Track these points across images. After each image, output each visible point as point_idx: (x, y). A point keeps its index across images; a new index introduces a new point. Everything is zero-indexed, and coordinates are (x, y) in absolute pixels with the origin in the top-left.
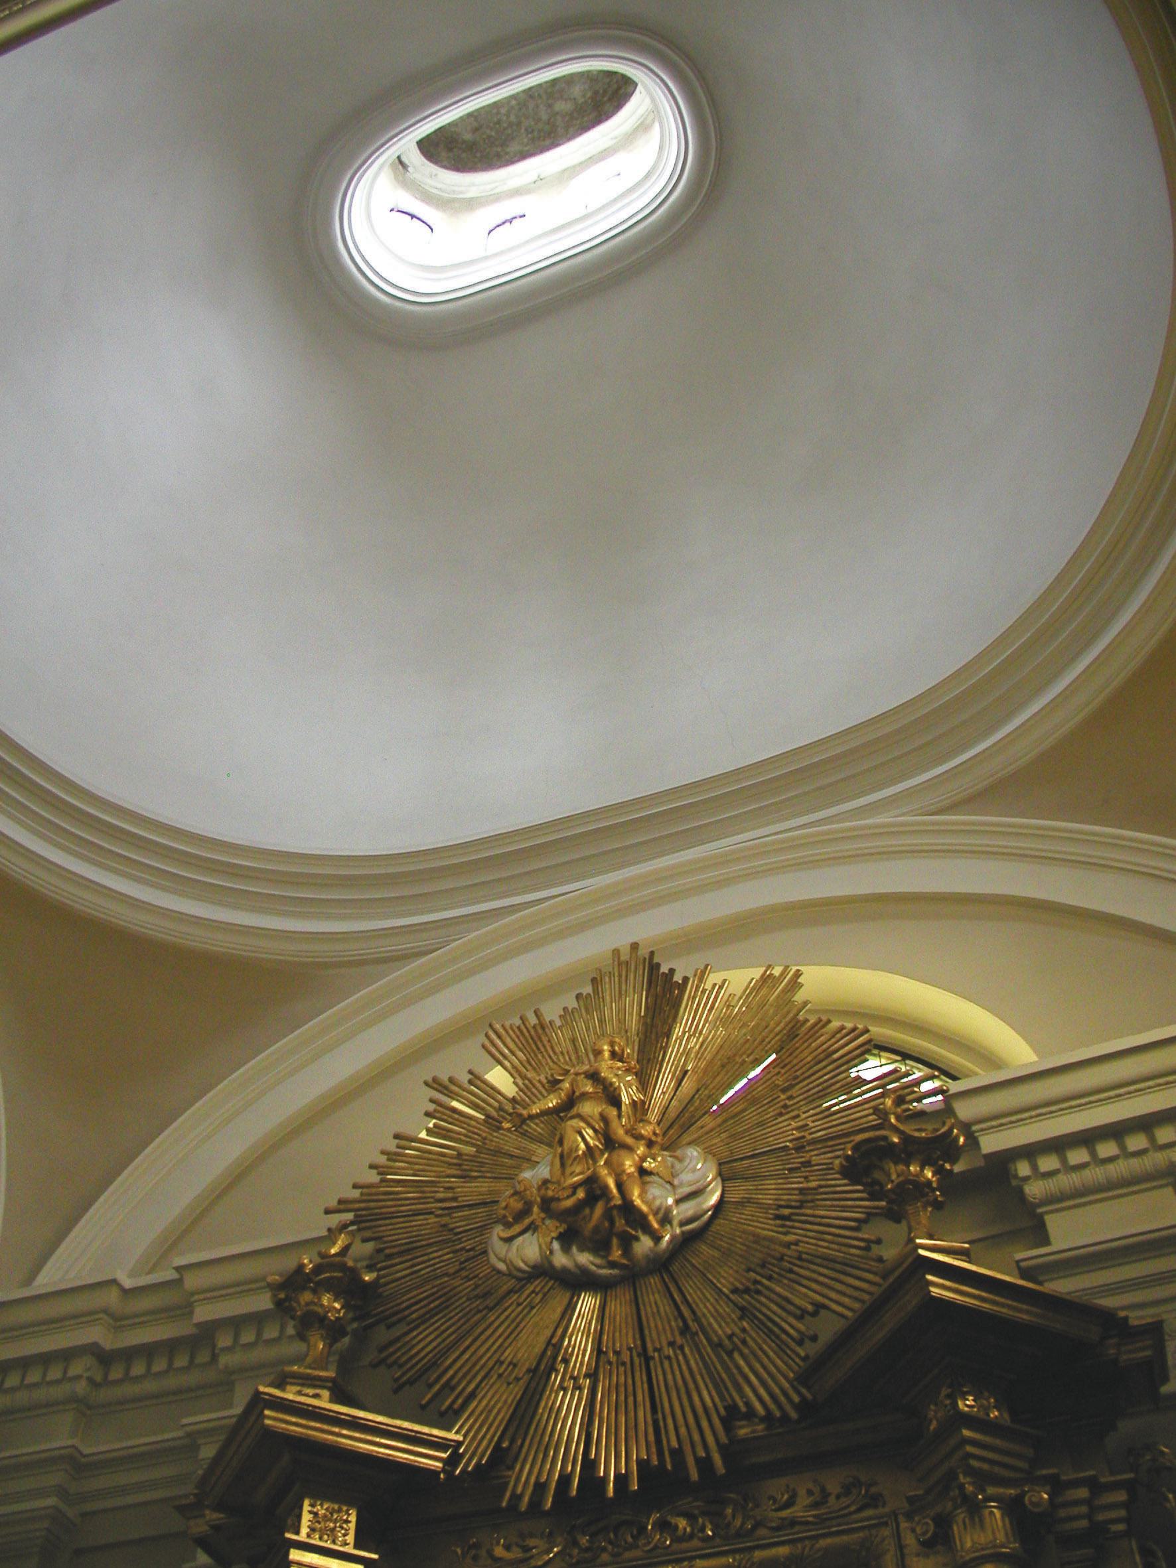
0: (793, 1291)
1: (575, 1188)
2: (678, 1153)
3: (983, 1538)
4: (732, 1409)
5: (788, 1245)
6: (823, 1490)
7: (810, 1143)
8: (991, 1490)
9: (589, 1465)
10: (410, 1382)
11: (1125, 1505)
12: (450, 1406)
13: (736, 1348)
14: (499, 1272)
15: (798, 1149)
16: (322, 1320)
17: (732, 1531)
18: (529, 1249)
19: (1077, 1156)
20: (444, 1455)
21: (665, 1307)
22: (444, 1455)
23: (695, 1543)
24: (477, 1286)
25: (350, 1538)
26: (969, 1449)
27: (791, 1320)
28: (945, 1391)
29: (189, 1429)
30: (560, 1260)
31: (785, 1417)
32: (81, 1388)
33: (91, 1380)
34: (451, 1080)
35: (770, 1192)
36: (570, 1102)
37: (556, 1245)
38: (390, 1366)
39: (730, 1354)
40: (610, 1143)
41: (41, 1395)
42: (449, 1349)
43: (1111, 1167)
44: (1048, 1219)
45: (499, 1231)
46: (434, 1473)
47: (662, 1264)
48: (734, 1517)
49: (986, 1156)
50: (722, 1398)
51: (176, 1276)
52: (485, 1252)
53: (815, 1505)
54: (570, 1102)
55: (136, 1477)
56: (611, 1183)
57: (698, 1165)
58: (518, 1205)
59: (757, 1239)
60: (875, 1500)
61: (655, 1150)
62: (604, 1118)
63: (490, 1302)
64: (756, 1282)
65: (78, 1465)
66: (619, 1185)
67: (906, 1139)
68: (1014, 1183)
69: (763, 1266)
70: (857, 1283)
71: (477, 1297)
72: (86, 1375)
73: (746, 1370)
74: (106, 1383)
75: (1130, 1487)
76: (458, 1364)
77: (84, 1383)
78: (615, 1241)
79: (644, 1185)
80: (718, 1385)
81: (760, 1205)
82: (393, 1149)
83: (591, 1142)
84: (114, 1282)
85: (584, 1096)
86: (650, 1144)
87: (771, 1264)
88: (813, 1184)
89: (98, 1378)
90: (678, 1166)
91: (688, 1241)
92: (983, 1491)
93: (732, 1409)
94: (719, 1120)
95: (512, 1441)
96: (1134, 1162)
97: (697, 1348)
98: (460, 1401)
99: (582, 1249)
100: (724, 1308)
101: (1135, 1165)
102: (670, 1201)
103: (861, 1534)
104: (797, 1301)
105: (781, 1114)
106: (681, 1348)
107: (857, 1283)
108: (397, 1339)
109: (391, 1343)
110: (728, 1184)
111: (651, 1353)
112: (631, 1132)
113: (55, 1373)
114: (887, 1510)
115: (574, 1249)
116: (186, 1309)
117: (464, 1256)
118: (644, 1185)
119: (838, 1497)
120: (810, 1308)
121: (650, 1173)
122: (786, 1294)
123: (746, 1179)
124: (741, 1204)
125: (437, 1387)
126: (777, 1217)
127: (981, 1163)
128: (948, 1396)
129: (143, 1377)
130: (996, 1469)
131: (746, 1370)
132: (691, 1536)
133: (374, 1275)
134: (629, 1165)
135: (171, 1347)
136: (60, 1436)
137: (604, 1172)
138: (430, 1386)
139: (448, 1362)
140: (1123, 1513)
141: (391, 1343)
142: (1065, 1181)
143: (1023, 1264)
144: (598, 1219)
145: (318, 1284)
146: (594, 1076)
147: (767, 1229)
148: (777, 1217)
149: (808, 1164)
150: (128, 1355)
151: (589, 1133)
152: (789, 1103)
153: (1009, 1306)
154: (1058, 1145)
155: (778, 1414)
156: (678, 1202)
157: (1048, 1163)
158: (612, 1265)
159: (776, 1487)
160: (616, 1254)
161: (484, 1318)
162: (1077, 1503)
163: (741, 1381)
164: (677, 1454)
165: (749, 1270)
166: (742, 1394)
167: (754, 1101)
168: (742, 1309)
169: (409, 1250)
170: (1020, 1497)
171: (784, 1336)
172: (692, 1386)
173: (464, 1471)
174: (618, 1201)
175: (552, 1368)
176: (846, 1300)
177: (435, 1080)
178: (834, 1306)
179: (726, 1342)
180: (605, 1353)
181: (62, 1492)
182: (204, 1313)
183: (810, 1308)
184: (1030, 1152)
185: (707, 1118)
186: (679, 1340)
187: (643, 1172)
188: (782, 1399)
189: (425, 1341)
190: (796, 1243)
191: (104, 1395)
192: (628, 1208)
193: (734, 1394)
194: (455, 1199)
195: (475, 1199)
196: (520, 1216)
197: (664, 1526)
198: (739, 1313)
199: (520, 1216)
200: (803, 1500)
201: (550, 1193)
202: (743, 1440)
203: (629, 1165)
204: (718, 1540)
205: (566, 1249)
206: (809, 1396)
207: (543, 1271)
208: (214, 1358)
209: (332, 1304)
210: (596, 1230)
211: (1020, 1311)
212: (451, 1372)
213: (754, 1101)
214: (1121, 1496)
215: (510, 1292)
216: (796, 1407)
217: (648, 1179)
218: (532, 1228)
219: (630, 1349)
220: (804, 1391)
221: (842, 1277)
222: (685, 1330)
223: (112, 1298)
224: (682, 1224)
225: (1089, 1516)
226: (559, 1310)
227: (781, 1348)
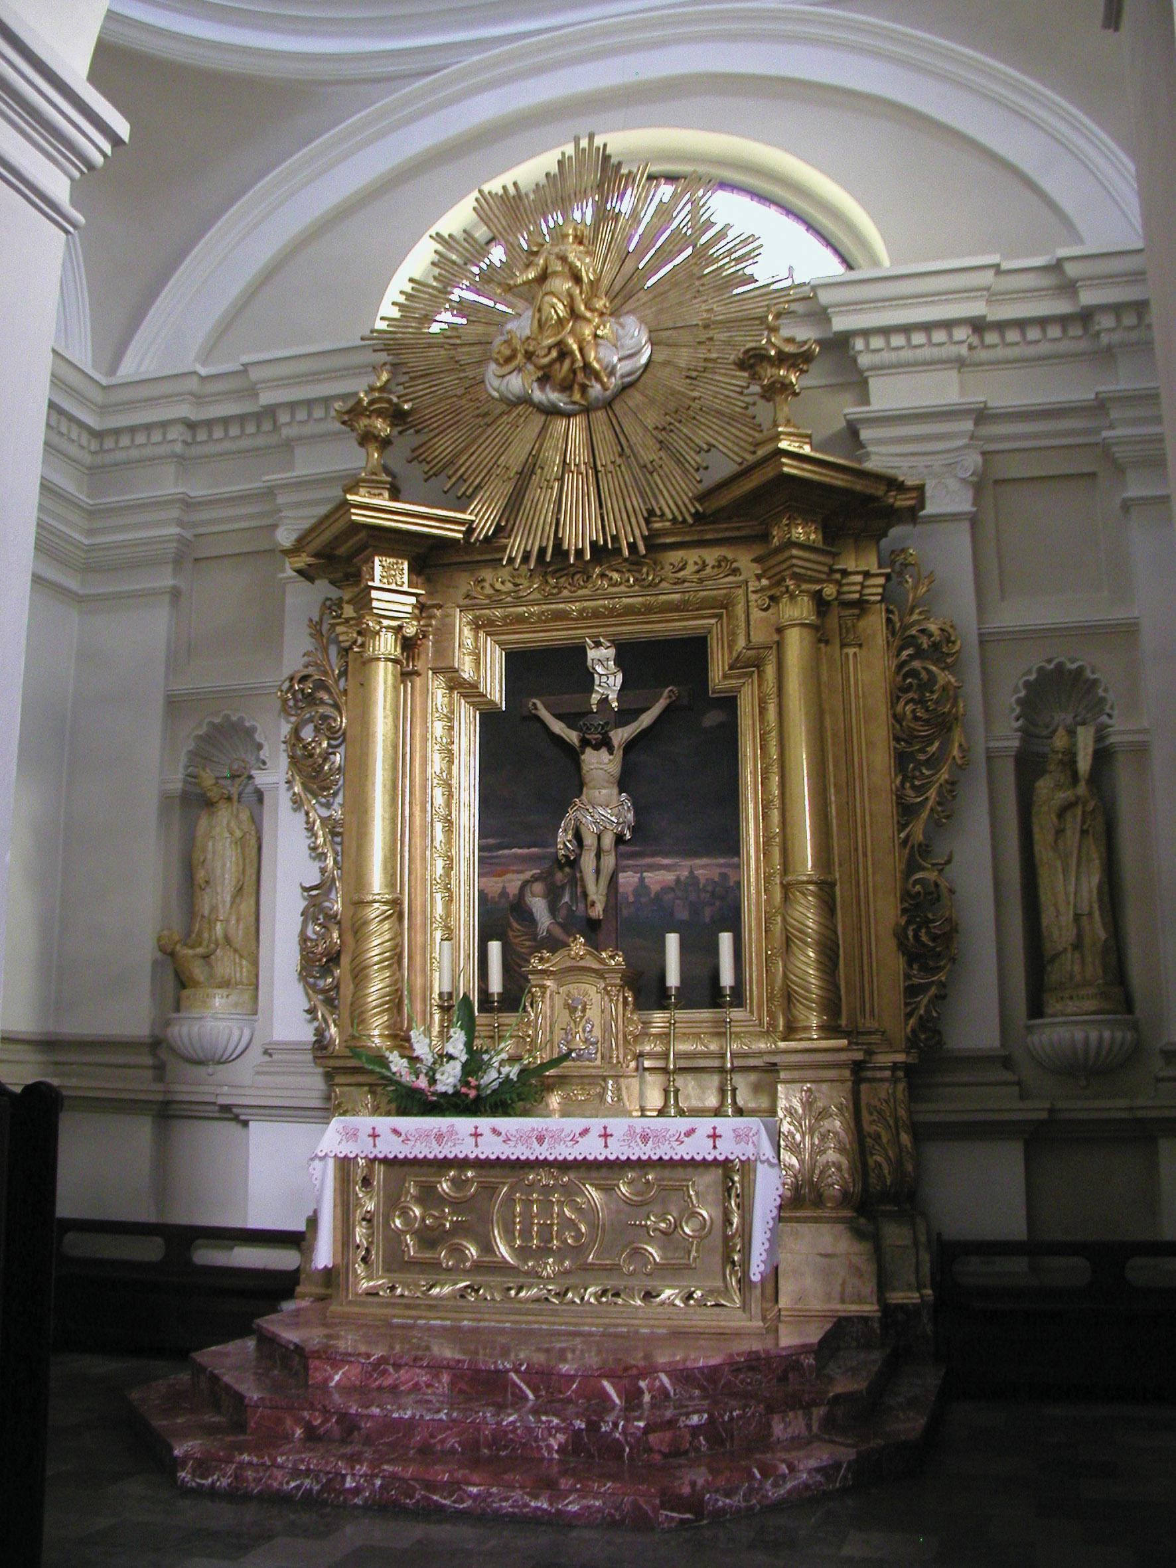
0: (695, 433)
1: (550, 349)
2: (622, 320)
3: (797, 613)
4: (651, 512)
5: (694, 399)
6: (704, 562)
7: (714, 322)
8: (804, 587)
9: (558, 542)
10: (435, 475)
11: (884, 586)
12: (464, 493)
13: (655, 470)
14: (493, 398)
15: (706, 327)
16: (376, 438)
17: (646, 583)
18: (516, 383)
19: (898, 340)
20: (463, 529)
21: (610, 436)
22: (463, 529)
23: (623, 588)
24: (478, 408)
25: (406, 585)
26: (795, 561)
27: (692, 453)
28: (785, 521)
29: (269, 484)
30: (538, 395)
31: (684, 521)
32: (178, 448)
33: (185, 442)
34: (450, 236)
35: (684, 357)
36: (543, 277)
37: (535, 385)
38: (420, 462)
39: (651, 473)
40: (574, 314)
41: (148, 452)
42: (461, 452)
43: (918, 351)
44: (871, 381)
45: (493, 366)
46: (457, 540)
47: (608, 404)
48: (648, 574)
49: (835, 333)
50: (645, 503)
51: (241, 368)
52: (483, 382)
53: (698, 572)
54: (543, 277)
55: (230, 512)
56: (575, 347)
57: (635, 333)
58: (508, 352)
59: (674, 393)
60: (735, 572)
61: (605, 318)
62: (571, 296)
63: (488, 420)
64: (670, 424)
65: (188, 504)
66: (581, 350)
67: (780, 352)
68: (852, 353)
69: (676, 412)
70: (738, 433)
71: (478, 416)
72: (181, 438)
73: (661, 486)
74: (195, 442)
75: (888, 577)
76: (468, 464)
77: (180, 444)
78: (576, 387)
79: (597, 345)
80: (643, 494)
81: (676, 367)
82: (409, 290)
83: (561, 314)
84: (195, 373)
85: (555, 273)
86: (602, 314)
87: (681, 411)
88: (714, 355)
89: (189, 440)
90: (621, 332)
91: (625, 388)
92: (799, 586)
93: (651, 512)
94: (650, 296)
95: (507, 522)
96: (935, 350)
97: (629, 466)
98: (471, 490)
99: (554, 390)
100: (650, 442)
101: (936, 352)
102: (615, 359)
103: (725, 591)
104: (697, 441)
105: (695, 297)
106: (619, 466)
107: (738, 433)
108: (425, 443)
109: (421, 446)
110: (655, 347)
111: (599, 468)
112: (588, 308)
113: (156, 437)
114: (741, 578)
115: (548, 388)
116: (252, 392)
117: (467, 383)
118: (597, 345)
119: (713, 567)
120: (705, 447)
121: (602, 338)
122: (691, 435)
123: (669, 345)
124: (666, 363)
125: (454, 479)
126: (688, 377)
127: (831, 335)
128: (787, 525)
129: (237, 437)
130: (809, 573)
131: (661, 486)
132: (621, 584)
133: (410, 404)
134: (588, 332)
135: (242, 419)
136: (169, 485)
137: (571, 341)
138: (450, 477)
139: (461, 462)
140: (880, 590)
141: (421, 446)
142: (888, 357)
143: (849, 417)
144: (566, 371)
145: (372, 412)
146: (563, 259)
147: (680, 385)
148: (688, 377)
149: (711, 339)
150: (209, 424)
151: (560, 306)
152: (701, 289)
153: (832, 477)
154: (886, 331)
155: (680, 519)
156: (620, 360)
157: (877, 342)
158: (574, 403)
159: (675, 556)
160: (577, 397)
161: (484, 432)
162: (854, 584)
163: (657, 491)
164: (615, 538)
165: (666, 414)
166: (658, 503)
167: (676, 284)
168: (661, 442)
169: (428, 374)
170: (820, 591)
171: (687, 465)
172: (625, 493)
173: (477, 539)
174: (580, 364)
175: (533, 472)
176: (730, 445)
177: (437, 234)
178: (721, 447)
179: (649, 466)
180: (569, 464)
181: (180, 523)
182: (267, 398)
183: (705, 447)
184: (866, 333)
185: (641, 294)
186: (619, 461)
187: (596, 336)
188: (684, 510)
189: (444, 446)
190: (699, 398)
191: (196, 450)
192: (587, 366)
193: (653, 502)
194: (459, 337)
195: (472, 339)
196: (509, 360)
197: (603, 576)
198: (658, 446)
199: (509, 360)
200: (691, 568)
201: (531, 348)
202: (657, 530)
203: (588, 332)
204: (637, 588)
205: (542, 389)
206: (701, 509)
207: (525, 400)
208: (276, 428)
209: (381, 426)
210: (564, 379)
211: (837, 478)
212: (463, 469)
213: (676, 284)
214: (881, 581)
215: (503, 413)
216: (692, 515)
217: (600, 341)
218: (519, 369)
219: (585, 463)
220: (698, 506)
221: (728, 427)
222: (621, 454)
223: (193, 384)
224: (622, 377)
225: (860, 592)
226: (537, 430)
227: (685, 472)
